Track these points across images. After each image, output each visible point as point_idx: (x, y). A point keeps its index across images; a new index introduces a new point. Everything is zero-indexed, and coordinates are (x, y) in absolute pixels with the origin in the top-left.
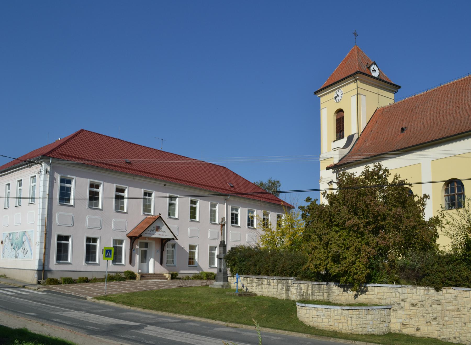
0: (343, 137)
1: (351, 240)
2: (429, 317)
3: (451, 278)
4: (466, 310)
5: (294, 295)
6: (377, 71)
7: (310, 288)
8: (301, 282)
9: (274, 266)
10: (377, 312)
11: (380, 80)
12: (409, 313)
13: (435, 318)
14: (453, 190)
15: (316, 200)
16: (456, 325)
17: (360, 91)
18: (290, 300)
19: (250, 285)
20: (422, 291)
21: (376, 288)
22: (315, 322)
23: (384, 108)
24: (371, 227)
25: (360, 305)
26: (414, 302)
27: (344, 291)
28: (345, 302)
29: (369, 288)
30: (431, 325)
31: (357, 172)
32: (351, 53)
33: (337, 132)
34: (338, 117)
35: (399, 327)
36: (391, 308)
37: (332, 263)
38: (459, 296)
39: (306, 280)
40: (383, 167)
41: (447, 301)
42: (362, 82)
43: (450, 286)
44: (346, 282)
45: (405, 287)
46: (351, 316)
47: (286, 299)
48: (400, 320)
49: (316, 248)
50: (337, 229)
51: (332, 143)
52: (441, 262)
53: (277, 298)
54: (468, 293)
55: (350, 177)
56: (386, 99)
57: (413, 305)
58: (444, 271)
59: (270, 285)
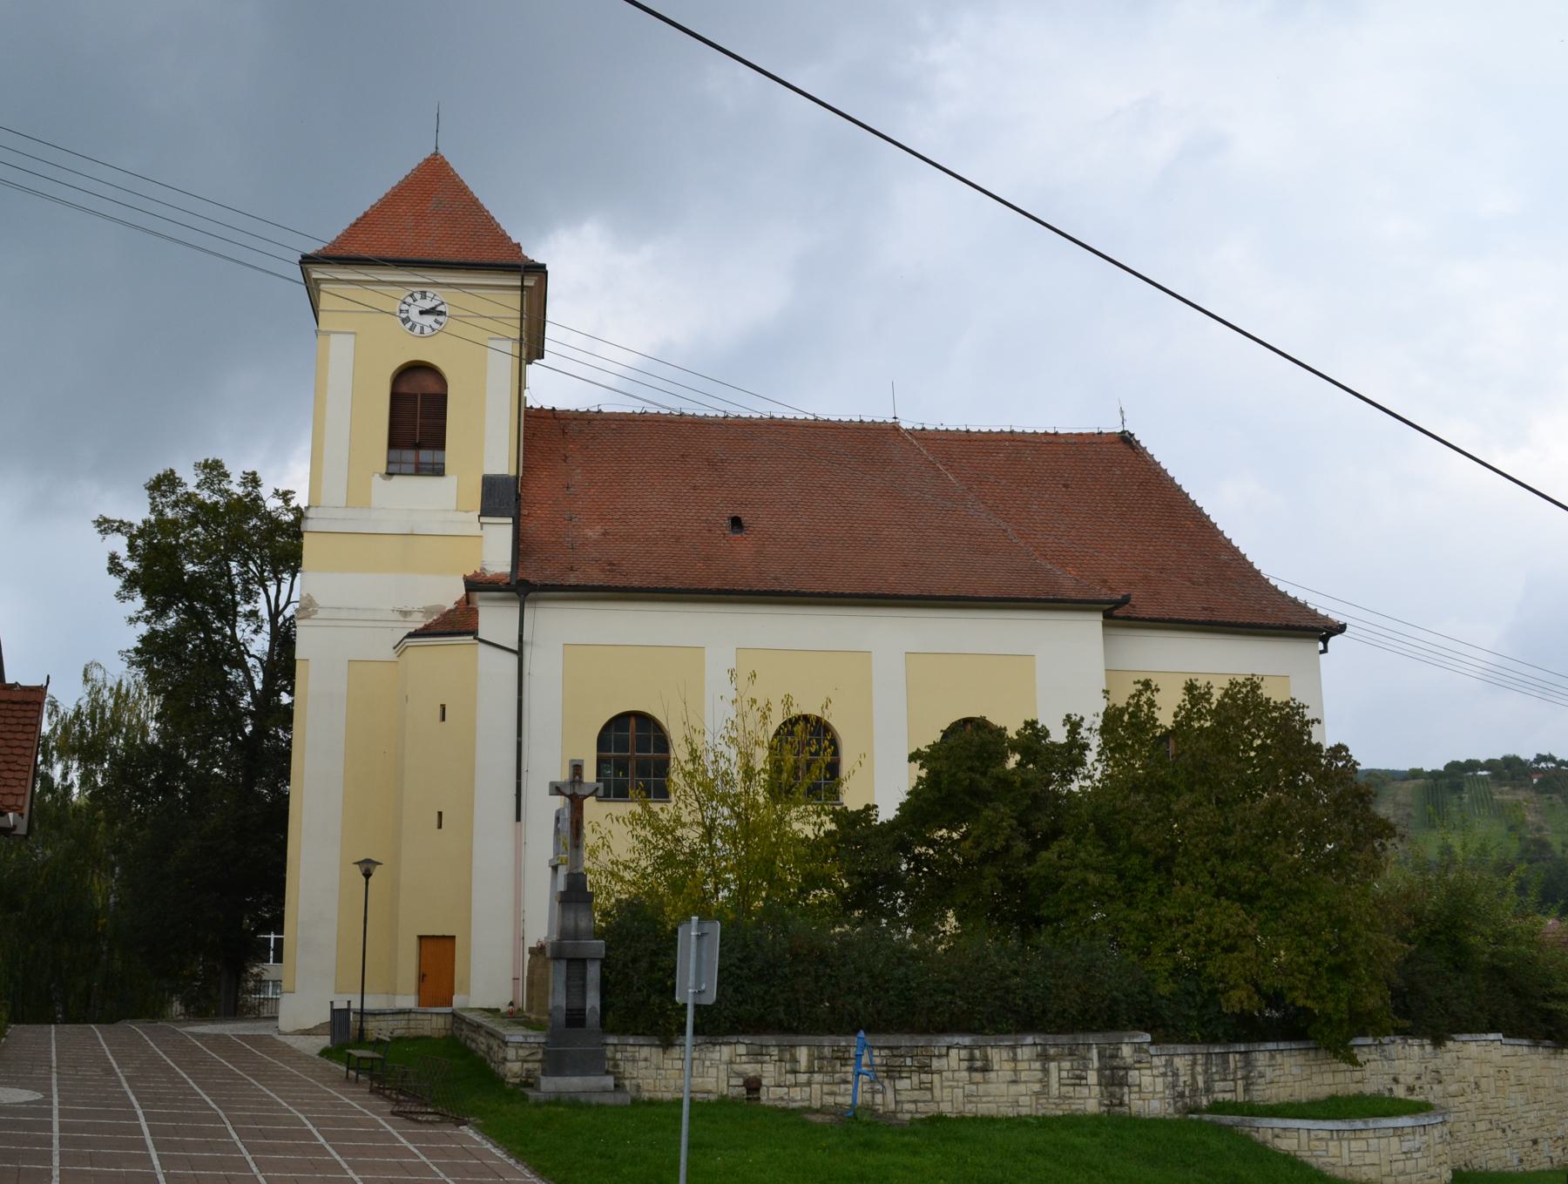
7: (1199, 1069)
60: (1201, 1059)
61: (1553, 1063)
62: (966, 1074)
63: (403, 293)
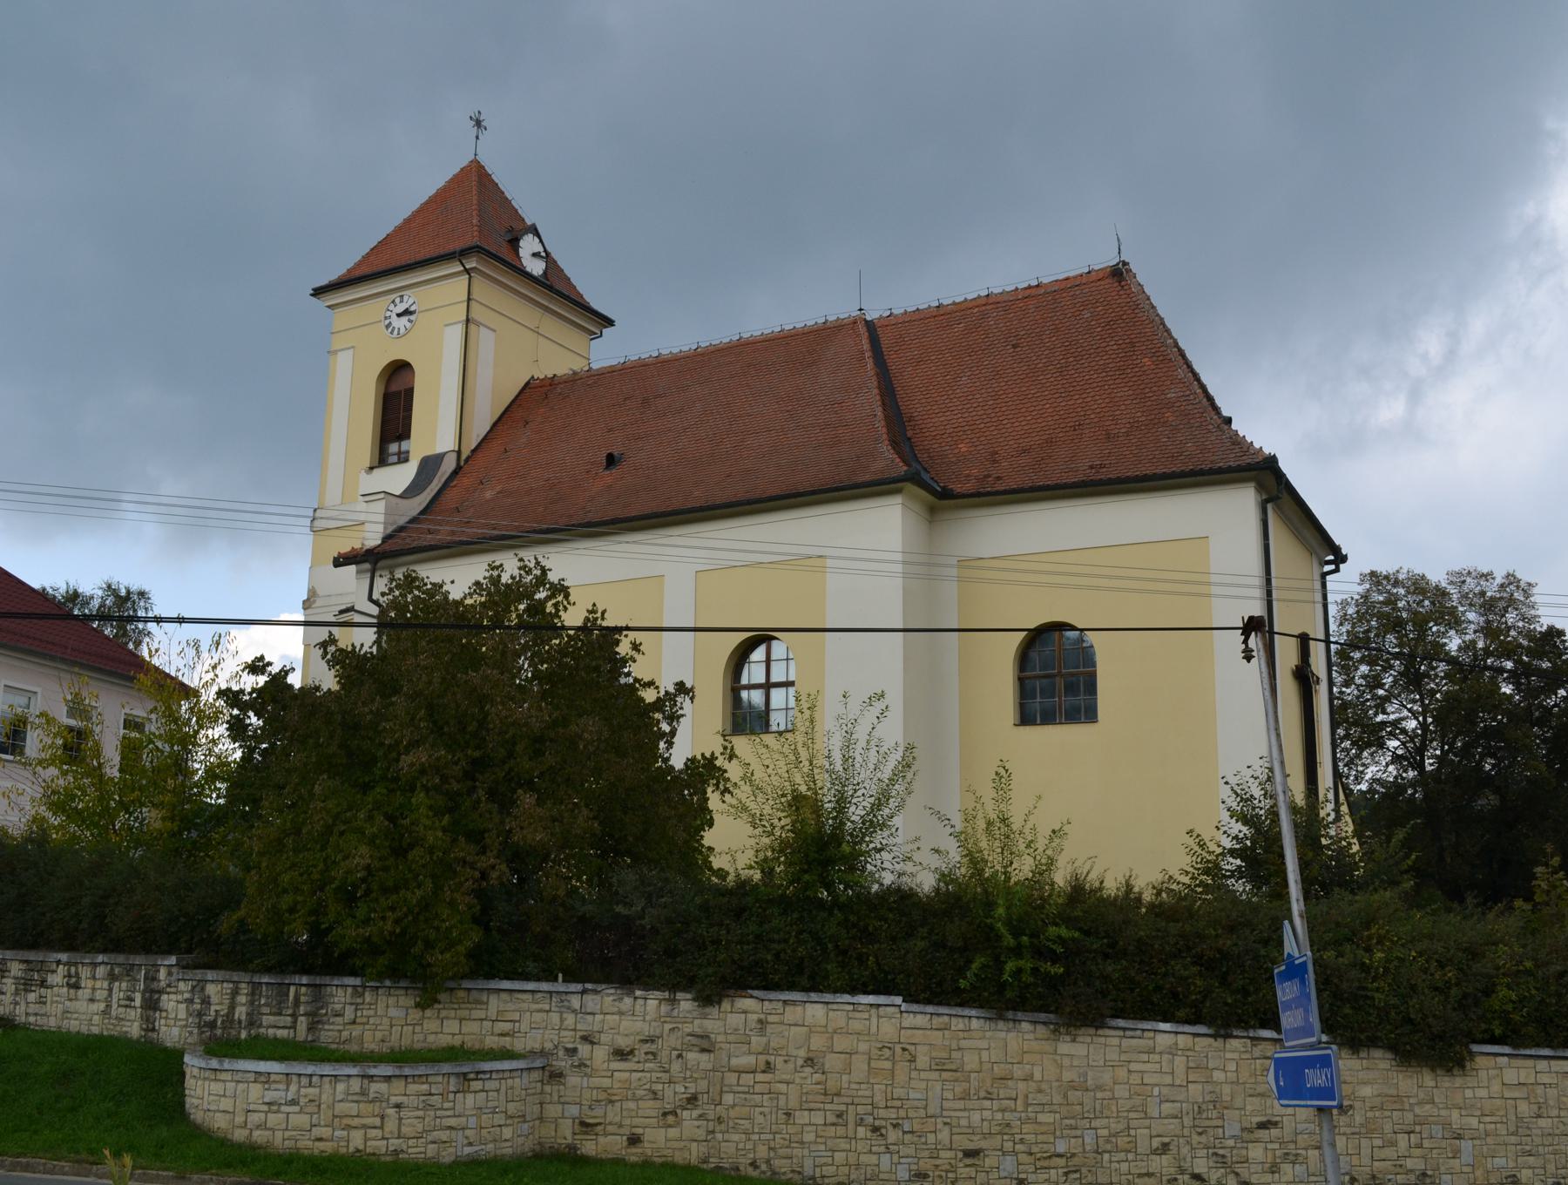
0: (403, 458)
2: (673, 1094)
7: (242, 999)
12: (606, 1082)
13: (692, 1100)
20: (652, 1004)
26: (623, 1042)
30: (678, 1124)
31: (459, 578)
41: (731, 1038)
45: (596, 992)
48: (574, 1110)
51: (363, 475)
54: (799, 1009)
57: (622, 1054)
59: (77, 986)
60: (244, 988)
61: (1065, 1047)
63: (384, 302)
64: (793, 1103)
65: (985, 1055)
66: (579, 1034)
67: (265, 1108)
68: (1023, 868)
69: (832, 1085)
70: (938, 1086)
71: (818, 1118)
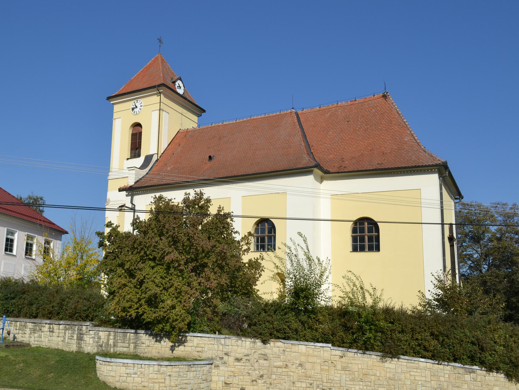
0: (139, 156)
1: (171, 279)
2: (255, 374)
3: (280, 329)
4: (294, 366)
5: (89, 345)
6: (182, 88)
7: (112, 337)
8: (101, 329)
9: (61, 305)
10: (199, 369)
11: (186, 99)
12: (233, 369)
13: (262, 376)
14: (263, 231)
15: (117, 227)
16: (284, 384)
17: (163, 106)
18: (83, 353)
19: (20, 332)
20: (248, 343)
21: (195, 338)
22: (123, 382)
23: (187, 131)
24: (191, 266)
25: (179, 359)
26: (239, 356)
27: (156, 341)
28: (156, 355)
29: (188, 338)
30: (257, 385)
31: (176, 197)
32: (154, 61)
33: (132, 149)
34: (135, 132)
35: (221, 387)
36: (212, 364)
37: (146, 307)
38: (288, 350)
39: (106, 327)
40: (205, 197)
41: (274, 356)
42: (166, 96)
43: (279, 338)
44: (162, 330)
45: (229, 338)
46: (170, 373)
47: (76, 352)
48: (222, 379)
49: (125, 285)
50: (153, 264)
51: (125, 161)
52: (269, 310)
53: (63, 351)
54: (297, 347)
55: (168, 203)
56: (189, 121)
57: (238, 360)
58: (272, 322)
59: (53, 332)
62: (48, 333)
64: (295, 379)
65: (360, 366)
66: (224, 352)
67: (126, 375)
68: (369, 301)
69: (309, 373)
70: (344, 376)
71: (304, 385)
